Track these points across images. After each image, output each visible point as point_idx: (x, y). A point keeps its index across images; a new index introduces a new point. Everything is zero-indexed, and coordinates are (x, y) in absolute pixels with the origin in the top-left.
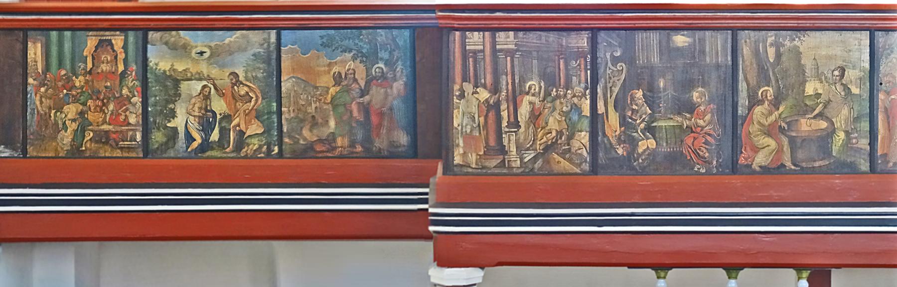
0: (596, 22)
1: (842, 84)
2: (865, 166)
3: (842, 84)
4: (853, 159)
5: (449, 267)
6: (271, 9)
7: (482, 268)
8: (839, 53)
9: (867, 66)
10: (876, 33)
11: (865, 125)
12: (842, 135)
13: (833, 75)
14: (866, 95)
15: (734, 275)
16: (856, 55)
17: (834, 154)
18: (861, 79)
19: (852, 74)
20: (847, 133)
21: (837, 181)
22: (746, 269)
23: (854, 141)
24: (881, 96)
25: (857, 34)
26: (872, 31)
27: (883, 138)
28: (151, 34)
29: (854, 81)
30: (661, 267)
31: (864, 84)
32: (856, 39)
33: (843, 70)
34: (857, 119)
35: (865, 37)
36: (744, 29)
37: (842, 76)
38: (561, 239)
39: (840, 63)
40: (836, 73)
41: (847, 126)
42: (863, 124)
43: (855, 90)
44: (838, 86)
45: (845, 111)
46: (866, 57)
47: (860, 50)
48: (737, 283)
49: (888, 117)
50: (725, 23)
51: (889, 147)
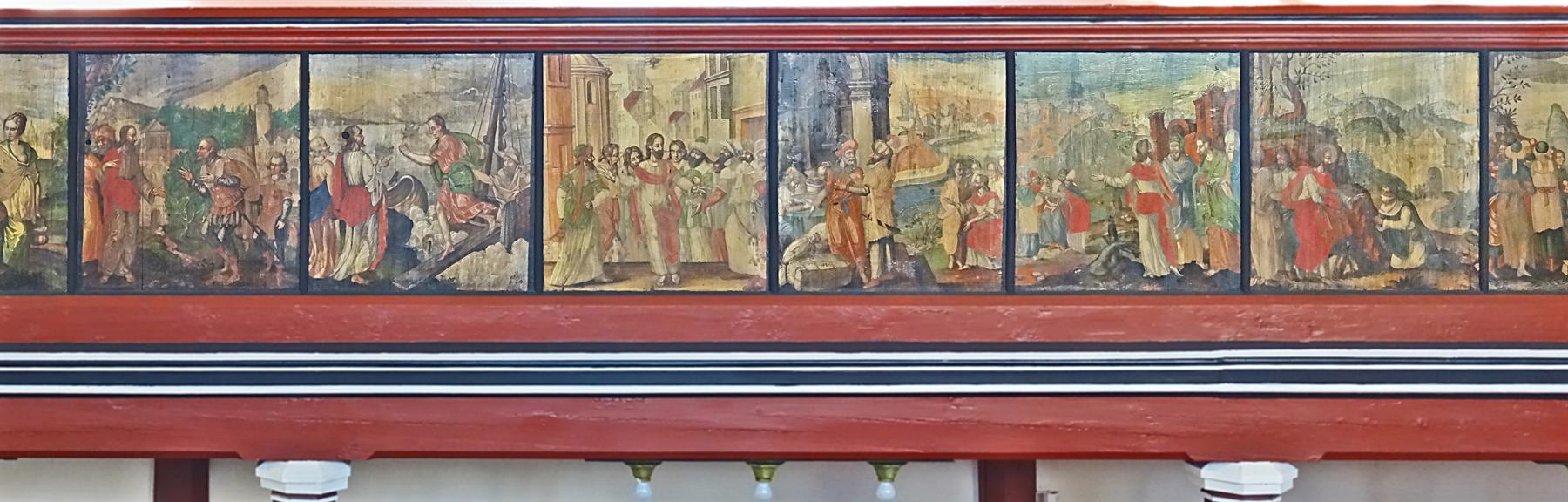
0: (774, 35)
1: (21, 143)
2: (58, 281)
3: (21, 143)
4: (38, 270)
5: (286, 460)
6: (208, 15)
7: (348, 462)
8: (16, 91)
9: (65, 112)
10: (81, 57)
11: (60, 212)
12: (20, 229)
13: (5, 128)
14: (62, 161)
15: (644, 473)
16: (43, 94)
17: (6, 261)
18: (53, 134)
19: (39, 127)
20: (29, 225)
21: (846, 310)
22: (787, 463)
23: (41, 238)
24: (89, 163)
25: (49, 59)
26: (773, 53)
27: (90, 234)
28: (1495, 58)
29: (41, 138)
30: (642, 462)
31: (60, 142)
32: (45, 66)
33: (22, 119)
34: (46, 202)
35: (61, 64)
36: (1264, 49)
37: (21, 129)
38: (651, 411)
39: (17, 107)
40: (11, 124)
41: (28, 213)
42: (56, 210)
43: (44, 153)
44: (14, 146)
45: (26, 188)
46: (63, 97)
47: (51, 86)
48: (772, 488)
49: (101, 199)
50: (992, 39)
51: (101, 249)
